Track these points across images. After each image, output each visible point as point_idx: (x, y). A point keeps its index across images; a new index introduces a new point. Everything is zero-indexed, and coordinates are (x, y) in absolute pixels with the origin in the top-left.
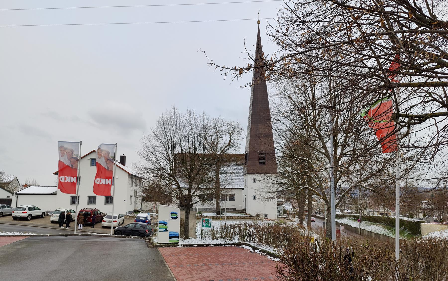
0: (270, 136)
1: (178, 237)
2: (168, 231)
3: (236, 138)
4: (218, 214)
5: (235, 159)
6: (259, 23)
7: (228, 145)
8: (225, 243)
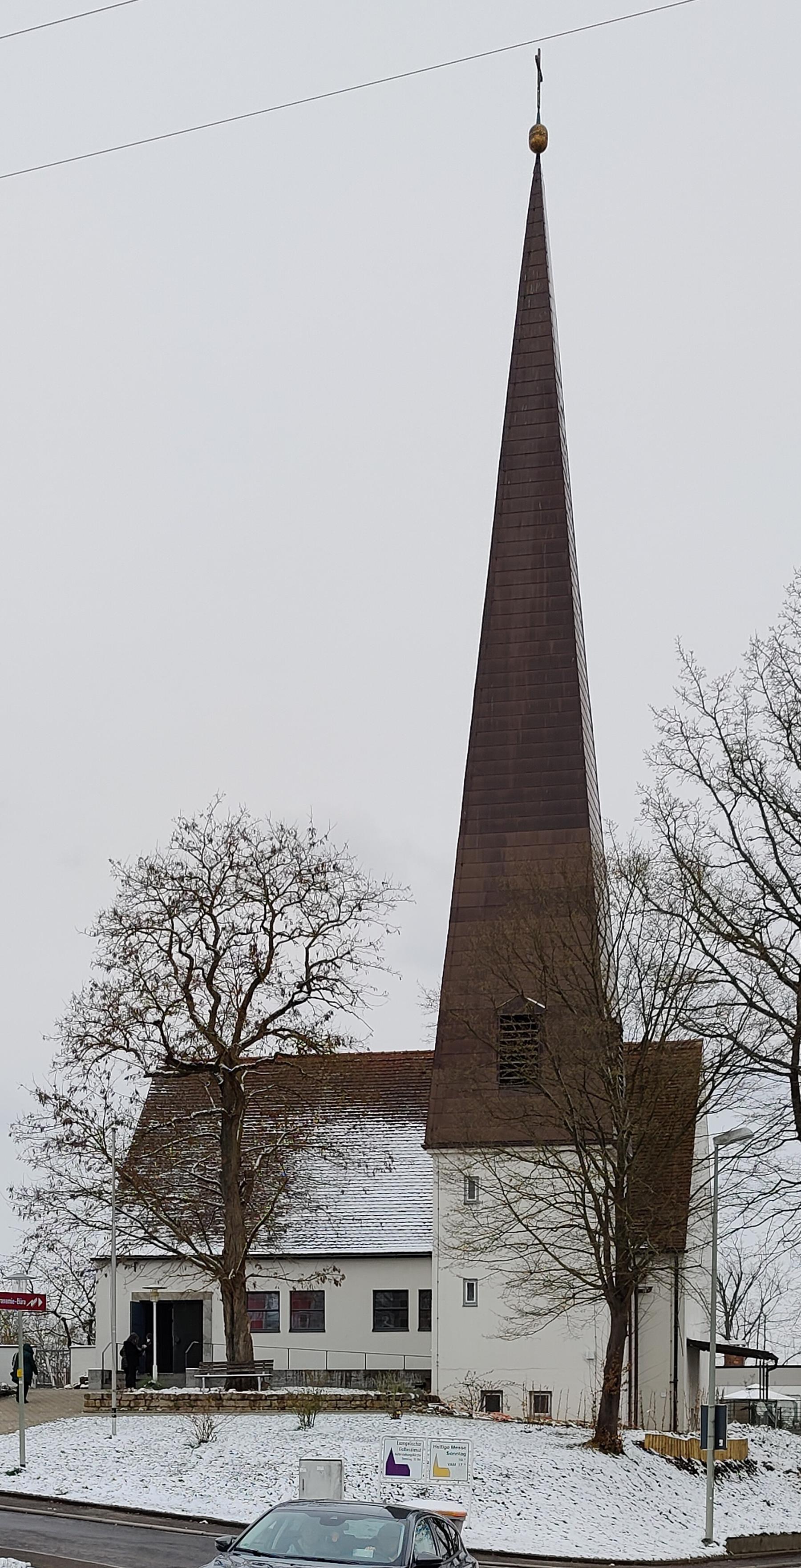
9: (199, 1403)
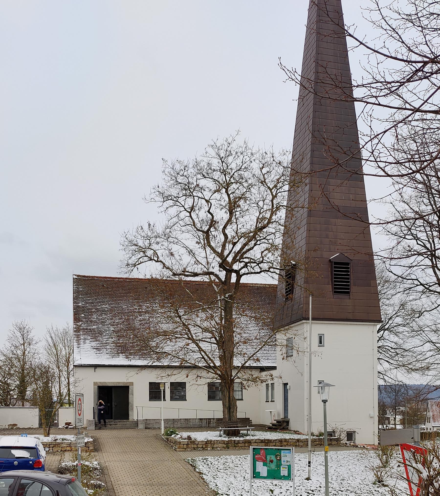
9: (239, 445)
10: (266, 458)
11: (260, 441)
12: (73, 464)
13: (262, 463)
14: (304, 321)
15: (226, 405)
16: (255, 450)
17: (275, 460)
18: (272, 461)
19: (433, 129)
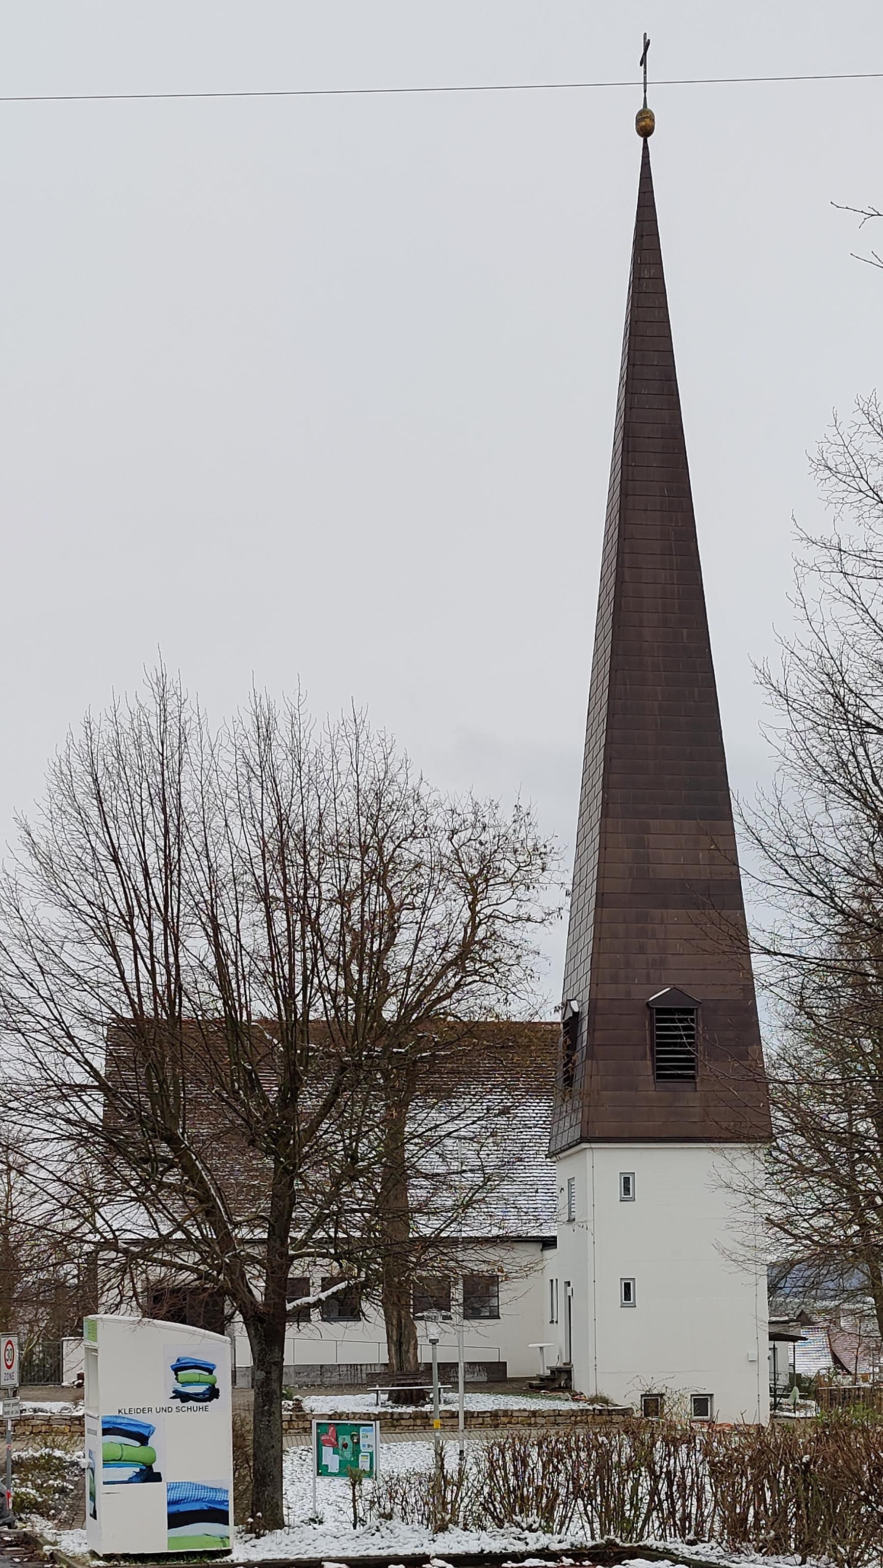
0: (722, 893)
1: (221, 1517)
2: (157, 1478)
3: (509, 908)
4: (397, 1398)
5: (505, 1048)
6: (645, 126)
7: (459, 962)
8: (520, 1547)
9: (403, 1422)
10: (337, 1440)
11: (448, 1415)
12: (35, 1454)
13: (331, 1449)
14: (584, 1145)
15: (392, 1339)
16: (321, 1427)
17: (350, 1444)
18: (345, 1446)
19: (325, 1005)
